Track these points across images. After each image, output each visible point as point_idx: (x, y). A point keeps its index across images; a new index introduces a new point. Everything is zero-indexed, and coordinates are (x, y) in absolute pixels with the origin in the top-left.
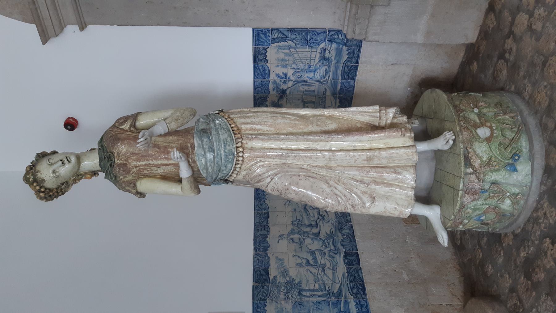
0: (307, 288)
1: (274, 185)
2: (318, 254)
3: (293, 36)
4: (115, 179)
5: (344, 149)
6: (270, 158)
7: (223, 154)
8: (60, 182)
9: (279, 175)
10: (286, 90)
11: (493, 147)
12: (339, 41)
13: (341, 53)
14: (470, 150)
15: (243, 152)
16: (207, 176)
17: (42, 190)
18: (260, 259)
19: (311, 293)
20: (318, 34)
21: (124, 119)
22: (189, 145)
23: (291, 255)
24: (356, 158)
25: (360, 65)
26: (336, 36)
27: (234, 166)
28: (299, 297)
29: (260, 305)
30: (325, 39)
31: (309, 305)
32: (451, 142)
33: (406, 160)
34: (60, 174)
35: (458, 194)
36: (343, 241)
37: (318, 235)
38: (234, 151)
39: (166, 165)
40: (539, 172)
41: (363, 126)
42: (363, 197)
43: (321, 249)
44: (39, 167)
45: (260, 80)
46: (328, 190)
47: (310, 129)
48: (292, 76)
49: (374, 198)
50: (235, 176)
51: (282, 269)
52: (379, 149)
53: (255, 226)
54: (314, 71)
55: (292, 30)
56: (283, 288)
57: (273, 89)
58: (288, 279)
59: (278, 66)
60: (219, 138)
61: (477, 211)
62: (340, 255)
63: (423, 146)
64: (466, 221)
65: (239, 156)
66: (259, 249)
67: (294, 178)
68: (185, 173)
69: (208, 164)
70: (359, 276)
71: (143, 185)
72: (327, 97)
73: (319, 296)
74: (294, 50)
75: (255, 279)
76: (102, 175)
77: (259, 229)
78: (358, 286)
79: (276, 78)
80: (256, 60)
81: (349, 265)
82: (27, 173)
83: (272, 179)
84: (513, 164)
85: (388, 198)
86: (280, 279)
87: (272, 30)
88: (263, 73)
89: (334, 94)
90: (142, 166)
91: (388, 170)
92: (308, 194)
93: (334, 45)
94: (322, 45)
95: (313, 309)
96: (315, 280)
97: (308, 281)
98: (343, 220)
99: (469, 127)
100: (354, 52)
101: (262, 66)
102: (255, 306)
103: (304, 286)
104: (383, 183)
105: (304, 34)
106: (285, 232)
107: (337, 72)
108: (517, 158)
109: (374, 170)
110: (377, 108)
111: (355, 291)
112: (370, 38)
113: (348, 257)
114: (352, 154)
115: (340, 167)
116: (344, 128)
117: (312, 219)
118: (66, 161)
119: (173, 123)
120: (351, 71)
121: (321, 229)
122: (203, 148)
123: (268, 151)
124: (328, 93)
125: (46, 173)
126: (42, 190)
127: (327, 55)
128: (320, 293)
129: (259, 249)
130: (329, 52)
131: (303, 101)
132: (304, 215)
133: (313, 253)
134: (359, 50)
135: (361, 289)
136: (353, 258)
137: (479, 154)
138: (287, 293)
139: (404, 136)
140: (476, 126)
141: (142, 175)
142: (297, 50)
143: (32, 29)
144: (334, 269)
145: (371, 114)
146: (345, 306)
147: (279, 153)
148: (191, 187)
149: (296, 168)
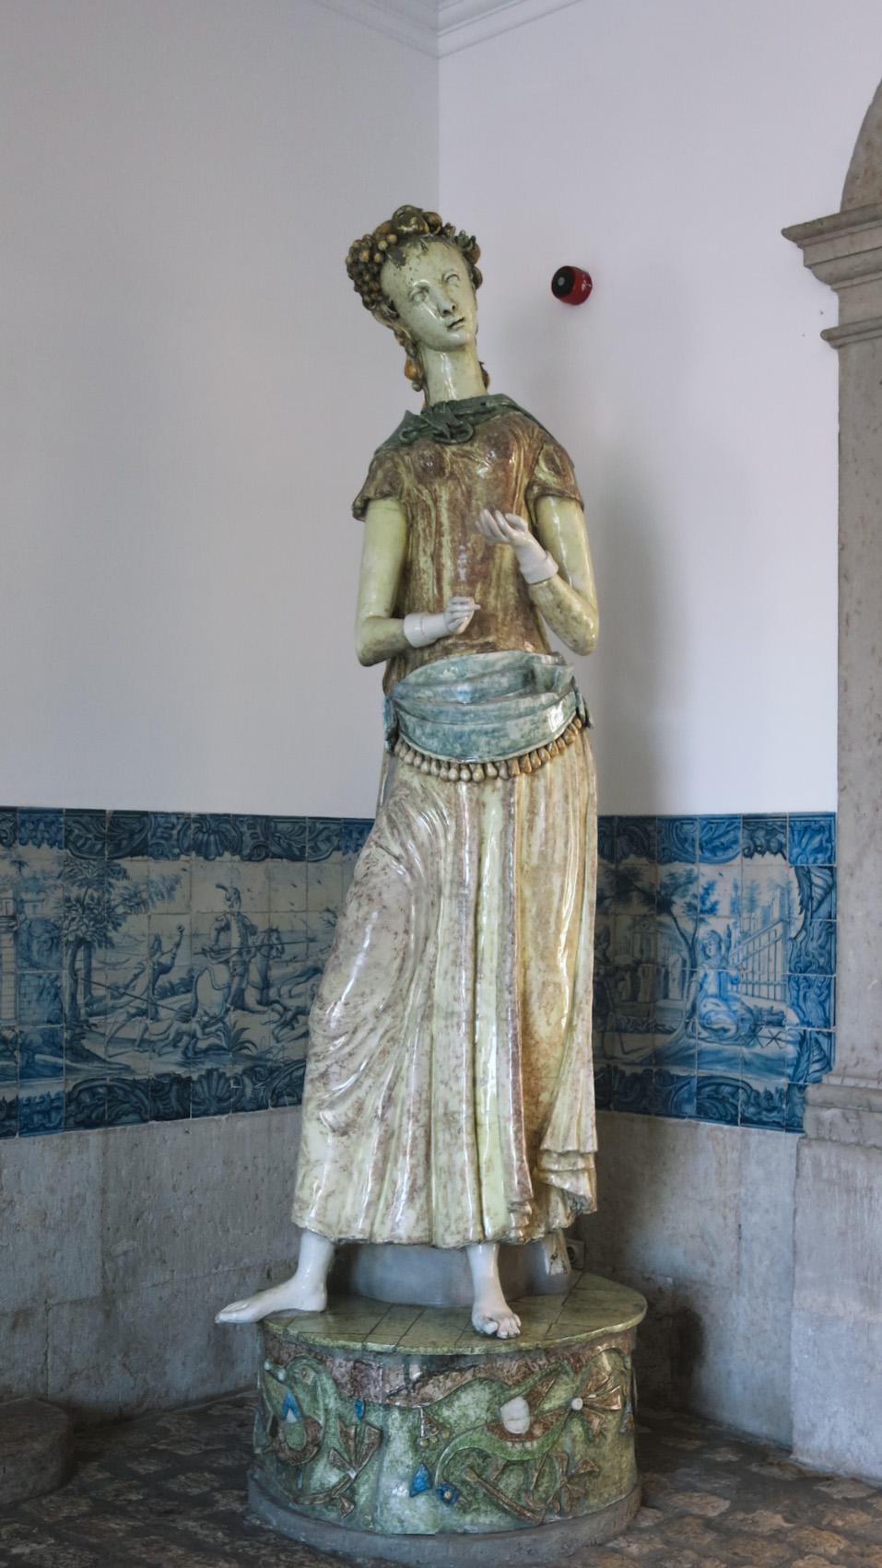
0: (95, 964)
1: (381, 865)
2: (184, 1000)
3: (816, 929)
4: (404, 444)
7: (468, 728)
8: (398, 302)
9: (408, 879)
10: (671, 914)
11: (476, 1436)
12: (803, 1065)
14: (469, 1375)
15: (471, 780)
16: (407, 684)
17: (378, 257)
19: (81, 974)
20: (822, 1004)
21: (560, 462)
22: (491, 639)
23: (184, 920)
24: (452, 1083)
25: (738, 1129)
26: (816, 1055)
28: (71, 938)
30: (809, 1024)
31: (51, 964)
32: (490, 1328)
33: (447, 1215)
36: (221, 1076)
37: (239, 1003)
38: (474, 758)
39: (439, 579)
40: (409, 1552)
41: (541, 1109)
43: (200, 1011)
44: (437, 248)
45: (697, 835)
46: (367, 1009)
47: (533, 964)
48: (709, 928)
49: (344, 1133)
50: (408, 759)
51: (145, 895)
52: (476, 1145)
53: (268, 818)
54: (722, 996)
55: (831, 929)
57: (672, 875)
58: (120, 910)
59: (736, 887)
60: (508, 717)
61: (308, 1399)
62: (181, 1065)
63: (485, 1265)
64: (281, 1376)
65: (459, 770)
66: (200, 830)
67: (402, 919)
68: (417, 628)
69: (441, 689)
70: (126, 1113)
71: (387, 516)
73: (73, 997)
76: (416, 403)
78: (99, 1107)
79: (703, 882)
80: (753, 822)
83: (397, 859)
84: (432, 1484)
85: (346, 1169)
86: (120, 886)
87: (831, 869)
88: (717, 843)
89: (659, 1057)
90: (438, 517)
92: (356, 954)
93: (791, 1051)
94: (792, 1017)
97: (114, 966)
98: (280, 1083)
99: (530, 1381)
100: (773, 1109)
101: (736, 842)
102: (51, 817)
103: (99, 954)
104: (385, 1159)
106: (246, 907)
107: (719, 1062)
108: (447, 1495)
109: (420, 1132)
110: (592, 1146)
111: (86, 1098)
112: (806, 1151)
114: (464, 1075)
115: (428, 1040)
116: (534, 1056)
117: (285, 990)
118: (451, 319)
119: (550, 597)
120: (722, 1104)
121: (257, 1017)
122: (483, 675)
123: (475, 848)
124: (661, 1040)
125: (421, 270)
126: (378, 257)
127: (765, 1031)
128: (80, 1000)
130: (774, 1038)
131: (638, 963)
132: (298, 967)
133: (189, 985)
134: (777, 1125)
139: (511, 1211)
140: (533, 1400)
143: (825, 200)
144: (143, 1043)
145: (574, 1131)
147: (469, 876)
148: (379, 642)
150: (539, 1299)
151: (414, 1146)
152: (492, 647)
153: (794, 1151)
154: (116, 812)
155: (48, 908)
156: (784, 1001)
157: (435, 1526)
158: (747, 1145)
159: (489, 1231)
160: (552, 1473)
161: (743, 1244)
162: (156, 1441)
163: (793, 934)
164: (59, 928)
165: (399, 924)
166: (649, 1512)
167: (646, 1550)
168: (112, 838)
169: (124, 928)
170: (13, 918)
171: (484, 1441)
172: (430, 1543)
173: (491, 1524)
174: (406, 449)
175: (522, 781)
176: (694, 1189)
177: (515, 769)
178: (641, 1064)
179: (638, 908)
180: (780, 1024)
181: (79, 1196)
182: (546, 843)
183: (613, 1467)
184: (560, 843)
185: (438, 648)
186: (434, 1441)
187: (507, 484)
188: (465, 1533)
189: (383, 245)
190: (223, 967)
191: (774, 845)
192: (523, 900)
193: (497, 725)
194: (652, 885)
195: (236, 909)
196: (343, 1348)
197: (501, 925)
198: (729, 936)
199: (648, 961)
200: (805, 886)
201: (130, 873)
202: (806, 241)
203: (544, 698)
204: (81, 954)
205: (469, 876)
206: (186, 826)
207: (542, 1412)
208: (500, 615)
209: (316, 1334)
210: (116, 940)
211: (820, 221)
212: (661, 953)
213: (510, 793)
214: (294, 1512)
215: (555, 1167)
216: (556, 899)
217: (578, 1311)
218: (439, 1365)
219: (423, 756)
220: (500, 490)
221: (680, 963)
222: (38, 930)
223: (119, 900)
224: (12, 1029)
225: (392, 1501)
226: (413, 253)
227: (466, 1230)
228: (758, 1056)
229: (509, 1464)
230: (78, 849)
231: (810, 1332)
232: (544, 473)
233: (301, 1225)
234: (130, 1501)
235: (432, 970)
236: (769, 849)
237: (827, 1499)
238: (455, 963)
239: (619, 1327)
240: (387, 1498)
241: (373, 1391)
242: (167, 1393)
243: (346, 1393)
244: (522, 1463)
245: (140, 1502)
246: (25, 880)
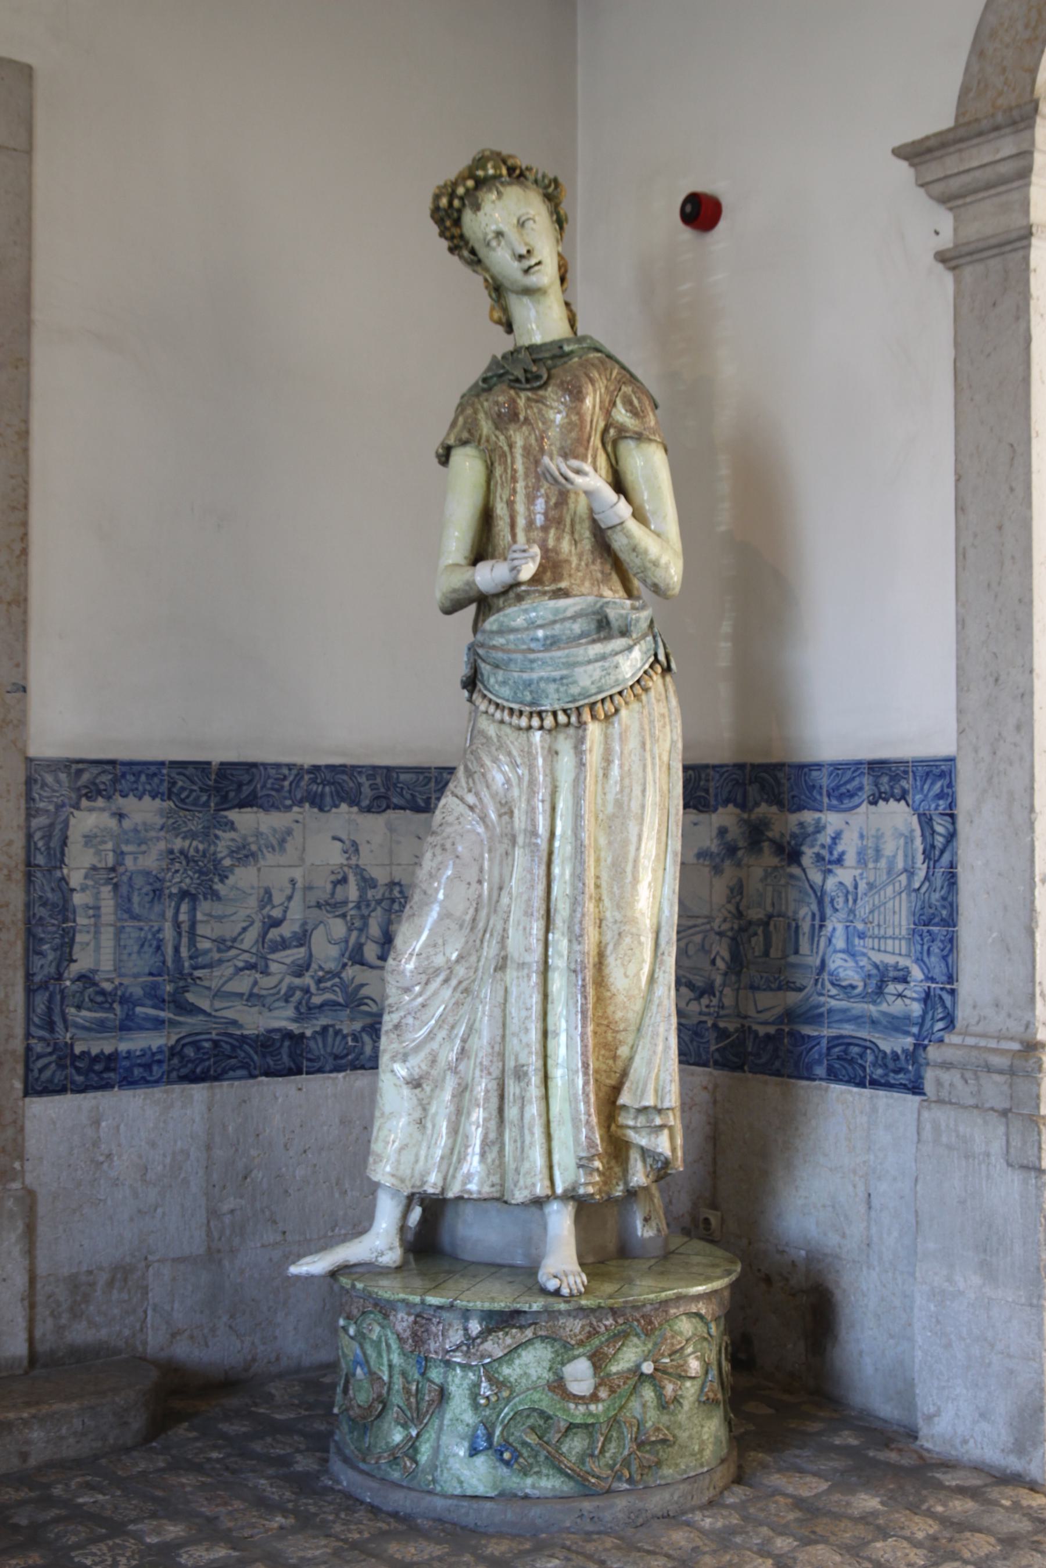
0: (199, 916)
1: (456, 814)
3: (938, 880)
5: (550, 1006)
6: (528, 801)
7: (535, 676)
8: (477, 247)
10: (800, 865)
11: (536, 1396)
12: (928, 1024)
13: (897, 1029)
14: (529, 1333)
16: (484, 632)
17: (456, 203)
18: (286, 783)
19: (185, 927)
20: (945, 958)
22: (563, 585)
23: (297, 874)
24: (522, 1035)
25: (867, 1092)
26: (940, 1013)
27: (506, 704)
28: (174, 890)
29: (156, 780)
30: (933, 980)
31: (153, 917)
32: (552, 1285)
34: (494, 249)
35: (412, 1294)
36: (337, 1032)
39: (513, 526)
40: (469, 1515)
42: (422, 1055)
43: (314, 966)
51: (254, 848)
53: (389, 769)
54: (850, 952)
55: (952, 879)
56: (201, 847)
57: (801, 825)
58: (227, 862)
59: (862, 837)
62: (295, 1020)
63: (561, 1222)
64: (352, 1331)
66: (314, 781)
67: (475, 869)
69: (512, 637)
70: (233, 1069)
71: (467, 465)
72: (780, 994)
73: (177, 950)
74: (904, 882)
75: (226, 768)
77: (379, 780)
78: (212, 1059)
79: (830, 831)
80: (877, 767)
81: (266, 1043)
82: (502, 159)
83: (471, 808)
86: (225, 840)
88: (843, 790)
89: (790, 1015)
91: (493, 1124)
93: (916, 1009)
94: (917, 973)
95: (141, 929)
96: (223, 941)
97: (220, 919)
99: (596, 1342)
102: (153, 769)
103: (205, 906)
105: (944, 913)
106: (365, 859)
107: (848, 1021)
108: (507, 1456)
109: (493, 1085)
111: (190, 1052)
112: (926, 1114)
113: (287, 1043)
115: (501, 993)
118: (526, 263)
120: (853, 1067)
122: (554, 622)
127: (891, 988)
128: (184, 953)
129: (314, 781)
130: (900, 995)
131: (770, 917)
133: (303, 938)
134: (904, 1088)
135: (193, 1071)
136: (285, 1058)
137: (519, 1356)
138: (186, 857)
139: (580, 1166)
140: (598, 1360)
141: (493, 461)
142: (904, 895)
143: (938, 116)
144: (253, 998)
146: (147, 1018)
148: (454, 591)
149: (501, 875)
150: (627, 1263)
151: (486, 1099)
152: (565, 593)
153: (915, 1116)
154: (222, 764)
155: (151, 861)
156: (908, 956)
157: (494, 1487)
158: (874, 1109)
159: (559, 1190)
160: (621, 1438)
161: (873, 1214)
162: (256, 1405)
163: (917, 885)
164: (161, 881)
165: (472, 874)
166: (738, 1489)
167: (719, 1524)
168: (218, 790)
169: (231, 881)
170: (113, 869)
171: (545, 1401)
172: (488, 1505)
173: (554, 1488)
174: (485, 395)
175: (594, 730)
176: (826, 1155)
177: (586, 716)
178: (773, 1023)
179: (769, 859)
180: (904, 980)
181: (182, 1151)
182: (622, 791)
183: (690, 1437)
184: (637, 790)
185: (512, 594)
186: (493, 1399)
187: (582, 428)
188: (526, 1497)
189: (461, 191)
190: (339, 921)
191: (897, 791)
192: (597, 849)
193: (565, 672)
194: (782, 835)
195: (353, 861)
196: (403, 1301)
197: (573, 875)
198: (856, 887)
199: (779, 916)
200: (927, 834)
201: (237, 825)
202: (916, 160)
203: (619, 643)
204: (184, 907)
205: (542, 828)
206: (299, 777)
207: (609, 1375)
208: (574, 561)
209: (388, 1289)
210: (222, 893)
211: (928, 138)
212: (792, 906)
213: (581, 740)
214: (362, 1472)
215: (631, 1123)
216: (632, 848)
217: (662, 1273)
218: (500, 1321)
219: (497, 705)
220: (573, 435)
221: (809, 918)
222: (139, 881)
223: (225, 852)
224: (110, 980)
225: (451, 1460)
226: (489, 198)
227: (534, 1185)
228: (884, 1014)
229: (571, 1427)
230: (183, 801)
231: (932, 1308)
232: (621, 415)
233: (376, 1178)
234: (209, 1460)
235: (506, 921)
236: (893, 796)
237: (940, 1486)
238: (528, 914)
239: (700, 1289)
240: (446, 1457)
241: (433, 1346)
242: (278, 1359)
243: (408, 1347)
244: (586, 1426)
245: (218, 1460)
246: (125, 832)
